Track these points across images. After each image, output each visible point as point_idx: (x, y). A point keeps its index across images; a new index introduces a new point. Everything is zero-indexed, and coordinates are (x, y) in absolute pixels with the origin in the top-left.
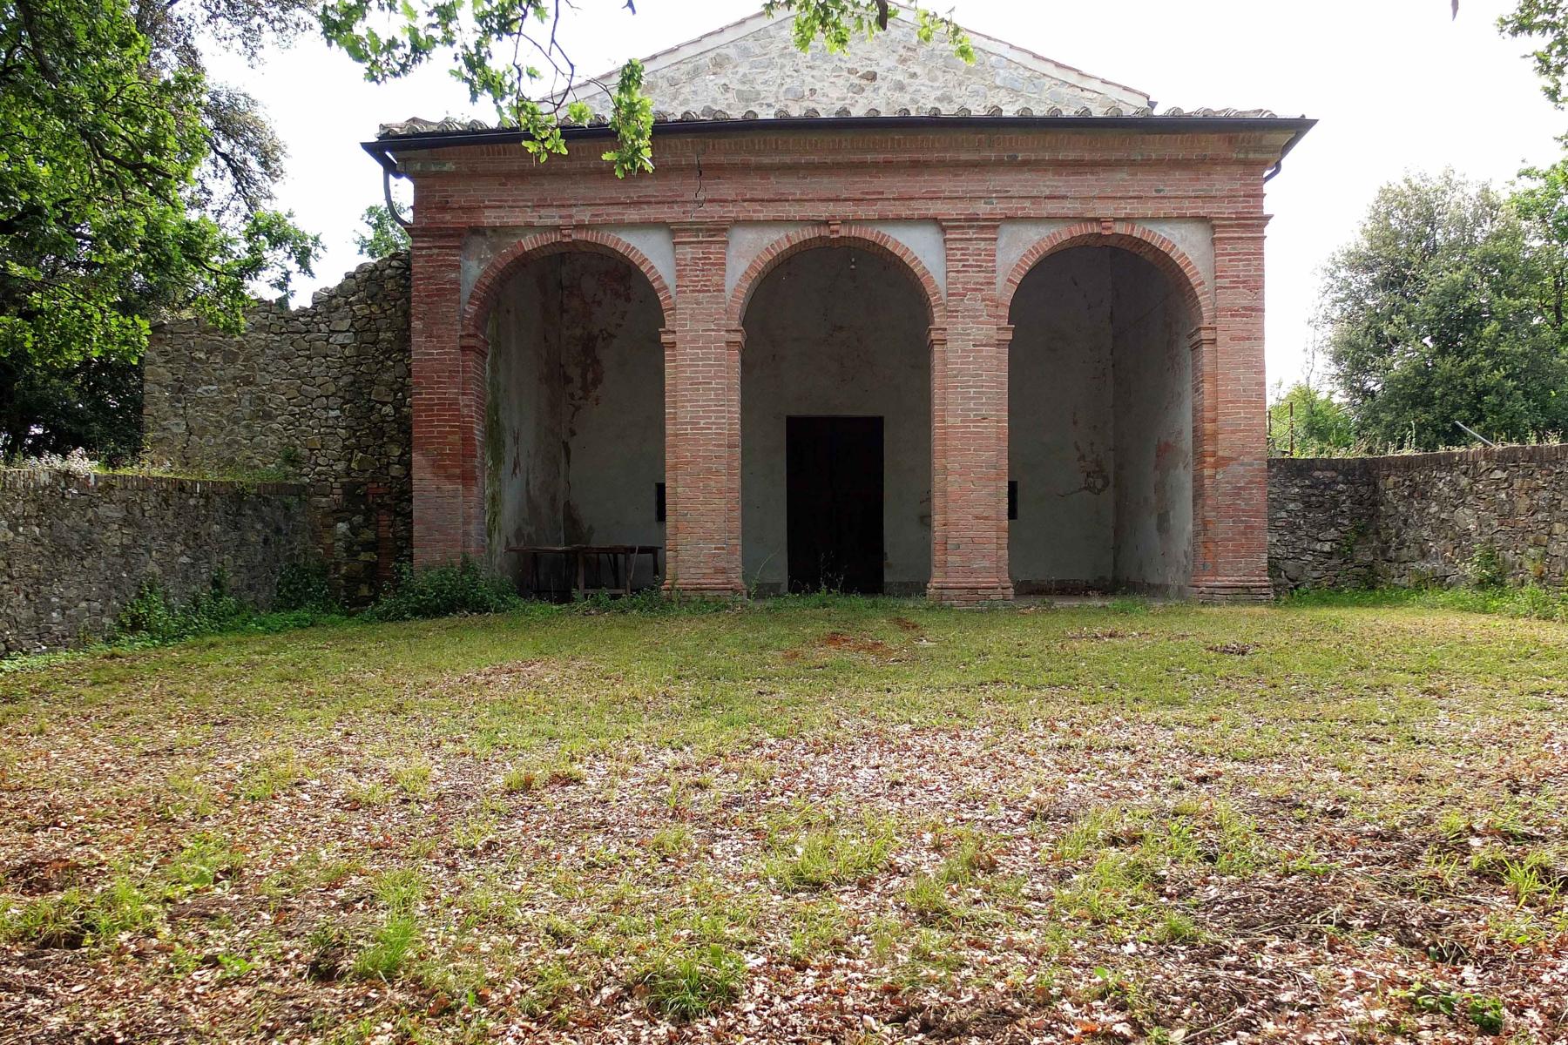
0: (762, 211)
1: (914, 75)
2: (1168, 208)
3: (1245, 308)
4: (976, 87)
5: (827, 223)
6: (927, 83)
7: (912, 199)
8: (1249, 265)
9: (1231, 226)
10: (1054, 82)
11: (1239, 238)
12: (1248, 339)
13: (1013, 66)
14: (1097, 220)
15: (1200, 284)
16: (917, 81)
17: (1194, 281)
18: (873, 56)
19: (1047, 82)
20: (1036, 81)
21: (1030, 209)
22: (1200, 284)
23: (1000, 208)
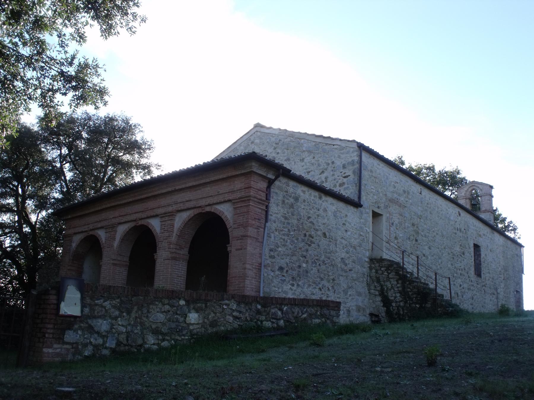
0: (122, 219)
1: (278, 153)
2: (221, 198)
3: (242, 236)
4: (297, 153)
5: (135, 221)
6: (282, 155)
7: (154, 209)
8: (244, 217)
9: (238, 202)
10: (323, 144)
11: (241, 207)
12: (242, 249)
13: (309, 141)
14: (200, 207)
15: (230, 228)
16: (279, 155)
17: (228, 227)
18: (266, 149)
19: (321, 145)
20: (317, 146)
21: (182, 207)
22: (230, 228)
23: (175, 207)
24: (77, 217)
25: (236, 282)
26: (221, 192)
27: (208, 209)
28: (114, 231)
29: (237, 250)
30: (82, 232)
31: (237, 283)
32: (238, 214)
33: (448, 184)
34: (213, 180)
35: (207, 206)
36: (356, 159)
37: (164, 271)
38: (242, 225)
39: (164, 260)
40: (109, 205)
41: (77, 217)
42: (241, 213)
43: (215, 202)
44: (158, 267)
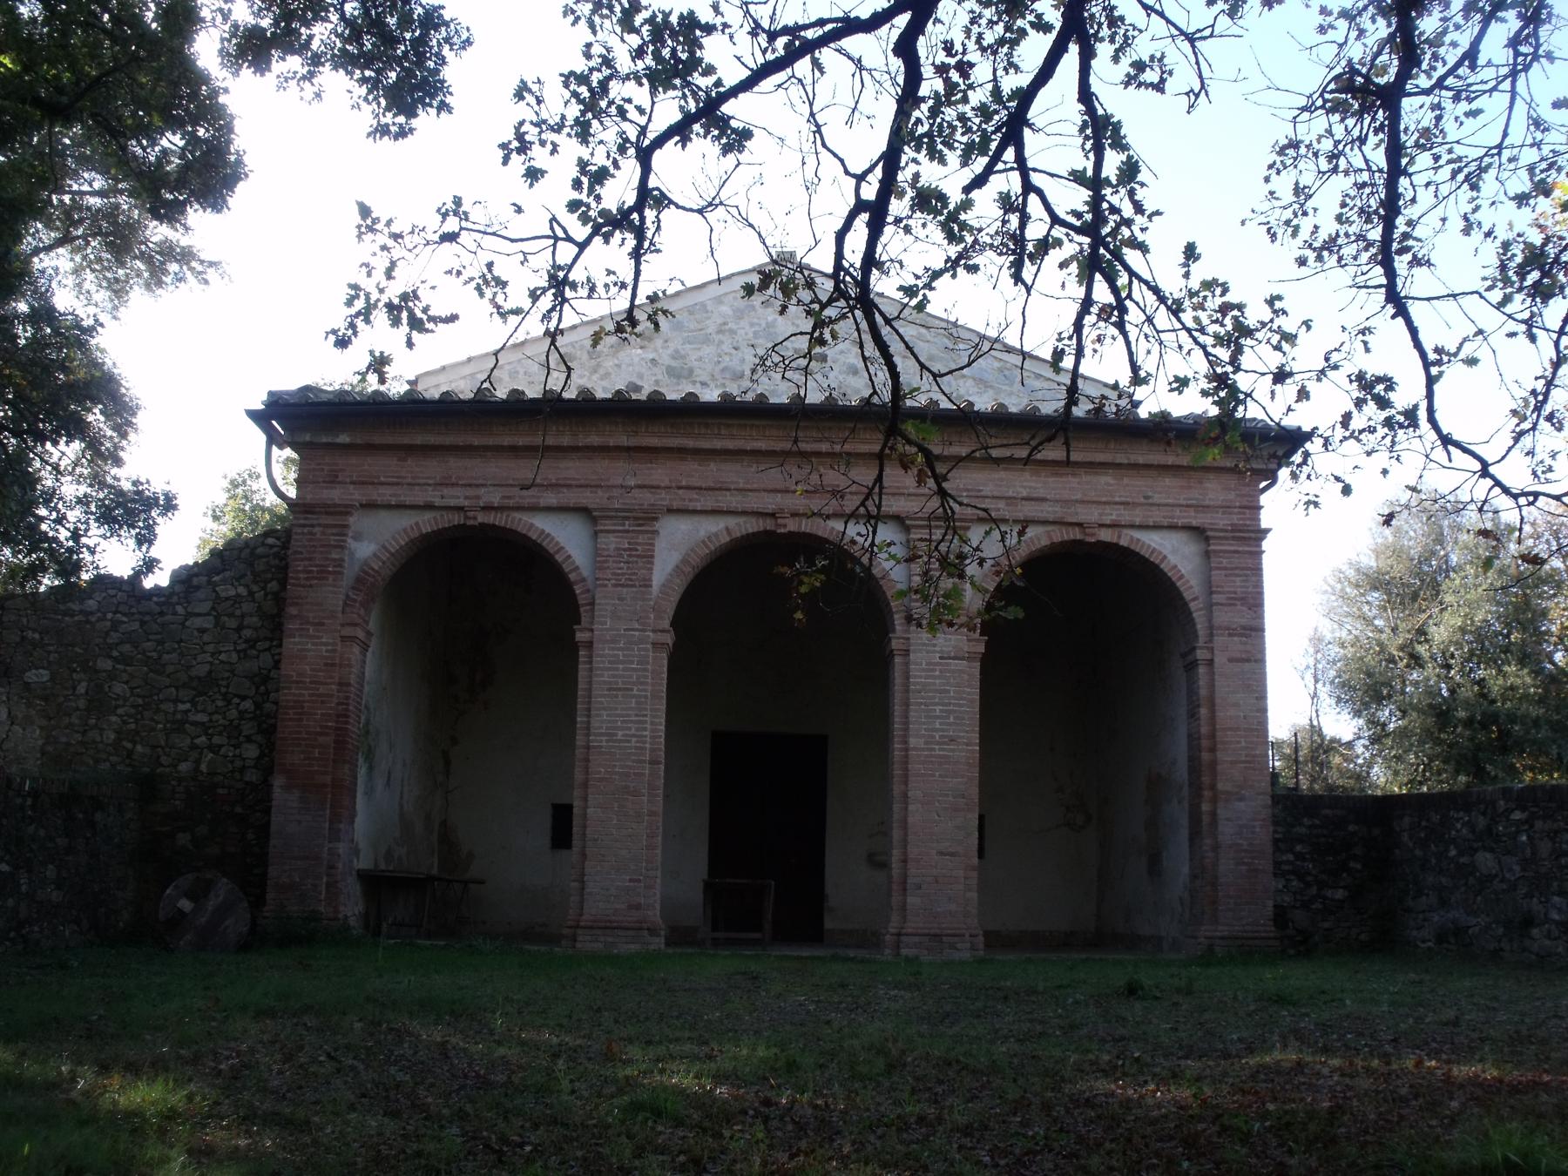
0: (697, 500)
2: (1157, 516)
3: (1244, 628)
14: (1080, 525)
17: (1187, 595)
24: (499, 450)
25: (1239, 742)
26: (1157, 499)
27: (1106, 536)
28: (647, 532)
29: (1231, 660)
30: (429, 507)
31: (1243, 744)
32: (1226, 569)
33: (157, 505)
34: (1141, 462)
35: (1102, 526)
36: (870, 485)
37: (948, 691)
38: (1242, 599)
39: (941, 658)
40: (507, 441)
41: (697, 452)
42: (1236, 568)
43: (1138, 521)
44: (916, 677)
